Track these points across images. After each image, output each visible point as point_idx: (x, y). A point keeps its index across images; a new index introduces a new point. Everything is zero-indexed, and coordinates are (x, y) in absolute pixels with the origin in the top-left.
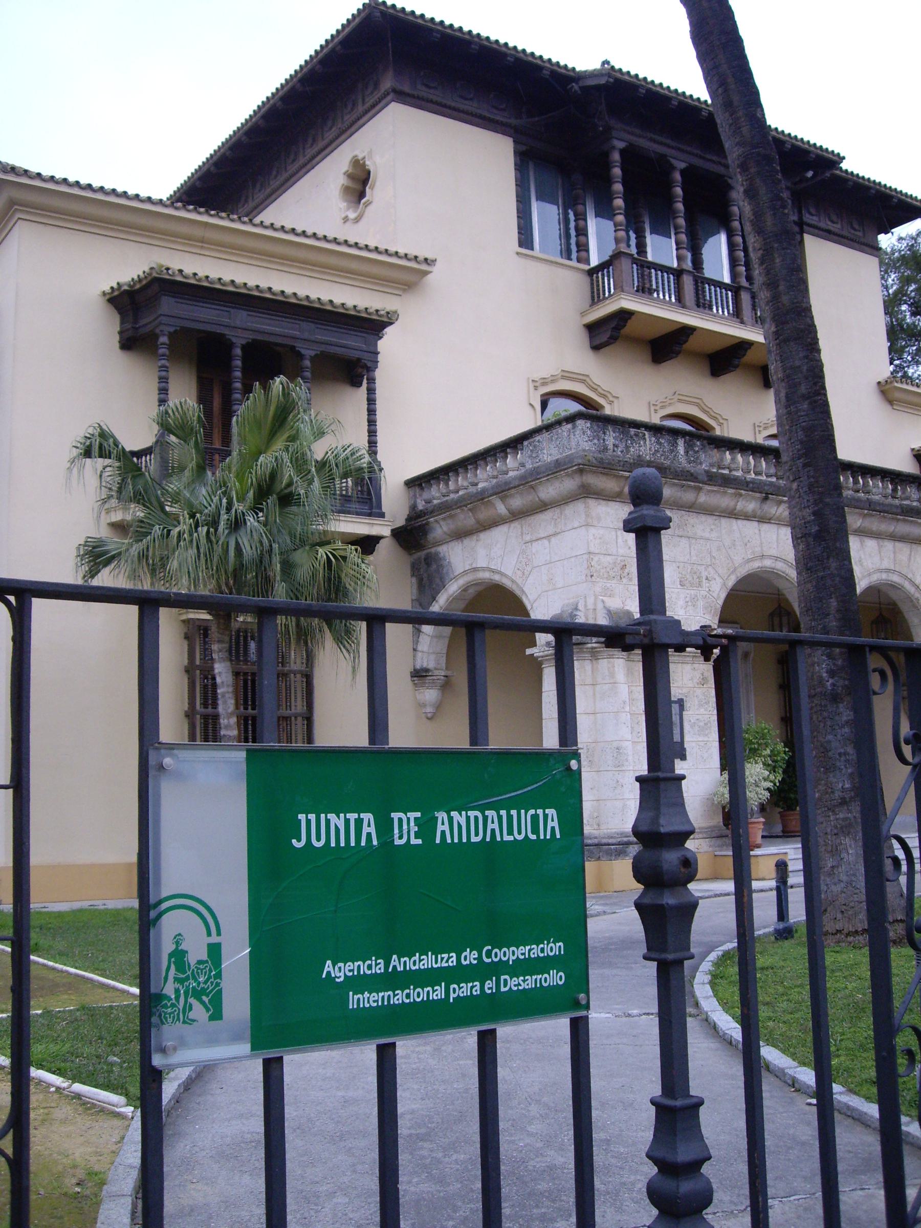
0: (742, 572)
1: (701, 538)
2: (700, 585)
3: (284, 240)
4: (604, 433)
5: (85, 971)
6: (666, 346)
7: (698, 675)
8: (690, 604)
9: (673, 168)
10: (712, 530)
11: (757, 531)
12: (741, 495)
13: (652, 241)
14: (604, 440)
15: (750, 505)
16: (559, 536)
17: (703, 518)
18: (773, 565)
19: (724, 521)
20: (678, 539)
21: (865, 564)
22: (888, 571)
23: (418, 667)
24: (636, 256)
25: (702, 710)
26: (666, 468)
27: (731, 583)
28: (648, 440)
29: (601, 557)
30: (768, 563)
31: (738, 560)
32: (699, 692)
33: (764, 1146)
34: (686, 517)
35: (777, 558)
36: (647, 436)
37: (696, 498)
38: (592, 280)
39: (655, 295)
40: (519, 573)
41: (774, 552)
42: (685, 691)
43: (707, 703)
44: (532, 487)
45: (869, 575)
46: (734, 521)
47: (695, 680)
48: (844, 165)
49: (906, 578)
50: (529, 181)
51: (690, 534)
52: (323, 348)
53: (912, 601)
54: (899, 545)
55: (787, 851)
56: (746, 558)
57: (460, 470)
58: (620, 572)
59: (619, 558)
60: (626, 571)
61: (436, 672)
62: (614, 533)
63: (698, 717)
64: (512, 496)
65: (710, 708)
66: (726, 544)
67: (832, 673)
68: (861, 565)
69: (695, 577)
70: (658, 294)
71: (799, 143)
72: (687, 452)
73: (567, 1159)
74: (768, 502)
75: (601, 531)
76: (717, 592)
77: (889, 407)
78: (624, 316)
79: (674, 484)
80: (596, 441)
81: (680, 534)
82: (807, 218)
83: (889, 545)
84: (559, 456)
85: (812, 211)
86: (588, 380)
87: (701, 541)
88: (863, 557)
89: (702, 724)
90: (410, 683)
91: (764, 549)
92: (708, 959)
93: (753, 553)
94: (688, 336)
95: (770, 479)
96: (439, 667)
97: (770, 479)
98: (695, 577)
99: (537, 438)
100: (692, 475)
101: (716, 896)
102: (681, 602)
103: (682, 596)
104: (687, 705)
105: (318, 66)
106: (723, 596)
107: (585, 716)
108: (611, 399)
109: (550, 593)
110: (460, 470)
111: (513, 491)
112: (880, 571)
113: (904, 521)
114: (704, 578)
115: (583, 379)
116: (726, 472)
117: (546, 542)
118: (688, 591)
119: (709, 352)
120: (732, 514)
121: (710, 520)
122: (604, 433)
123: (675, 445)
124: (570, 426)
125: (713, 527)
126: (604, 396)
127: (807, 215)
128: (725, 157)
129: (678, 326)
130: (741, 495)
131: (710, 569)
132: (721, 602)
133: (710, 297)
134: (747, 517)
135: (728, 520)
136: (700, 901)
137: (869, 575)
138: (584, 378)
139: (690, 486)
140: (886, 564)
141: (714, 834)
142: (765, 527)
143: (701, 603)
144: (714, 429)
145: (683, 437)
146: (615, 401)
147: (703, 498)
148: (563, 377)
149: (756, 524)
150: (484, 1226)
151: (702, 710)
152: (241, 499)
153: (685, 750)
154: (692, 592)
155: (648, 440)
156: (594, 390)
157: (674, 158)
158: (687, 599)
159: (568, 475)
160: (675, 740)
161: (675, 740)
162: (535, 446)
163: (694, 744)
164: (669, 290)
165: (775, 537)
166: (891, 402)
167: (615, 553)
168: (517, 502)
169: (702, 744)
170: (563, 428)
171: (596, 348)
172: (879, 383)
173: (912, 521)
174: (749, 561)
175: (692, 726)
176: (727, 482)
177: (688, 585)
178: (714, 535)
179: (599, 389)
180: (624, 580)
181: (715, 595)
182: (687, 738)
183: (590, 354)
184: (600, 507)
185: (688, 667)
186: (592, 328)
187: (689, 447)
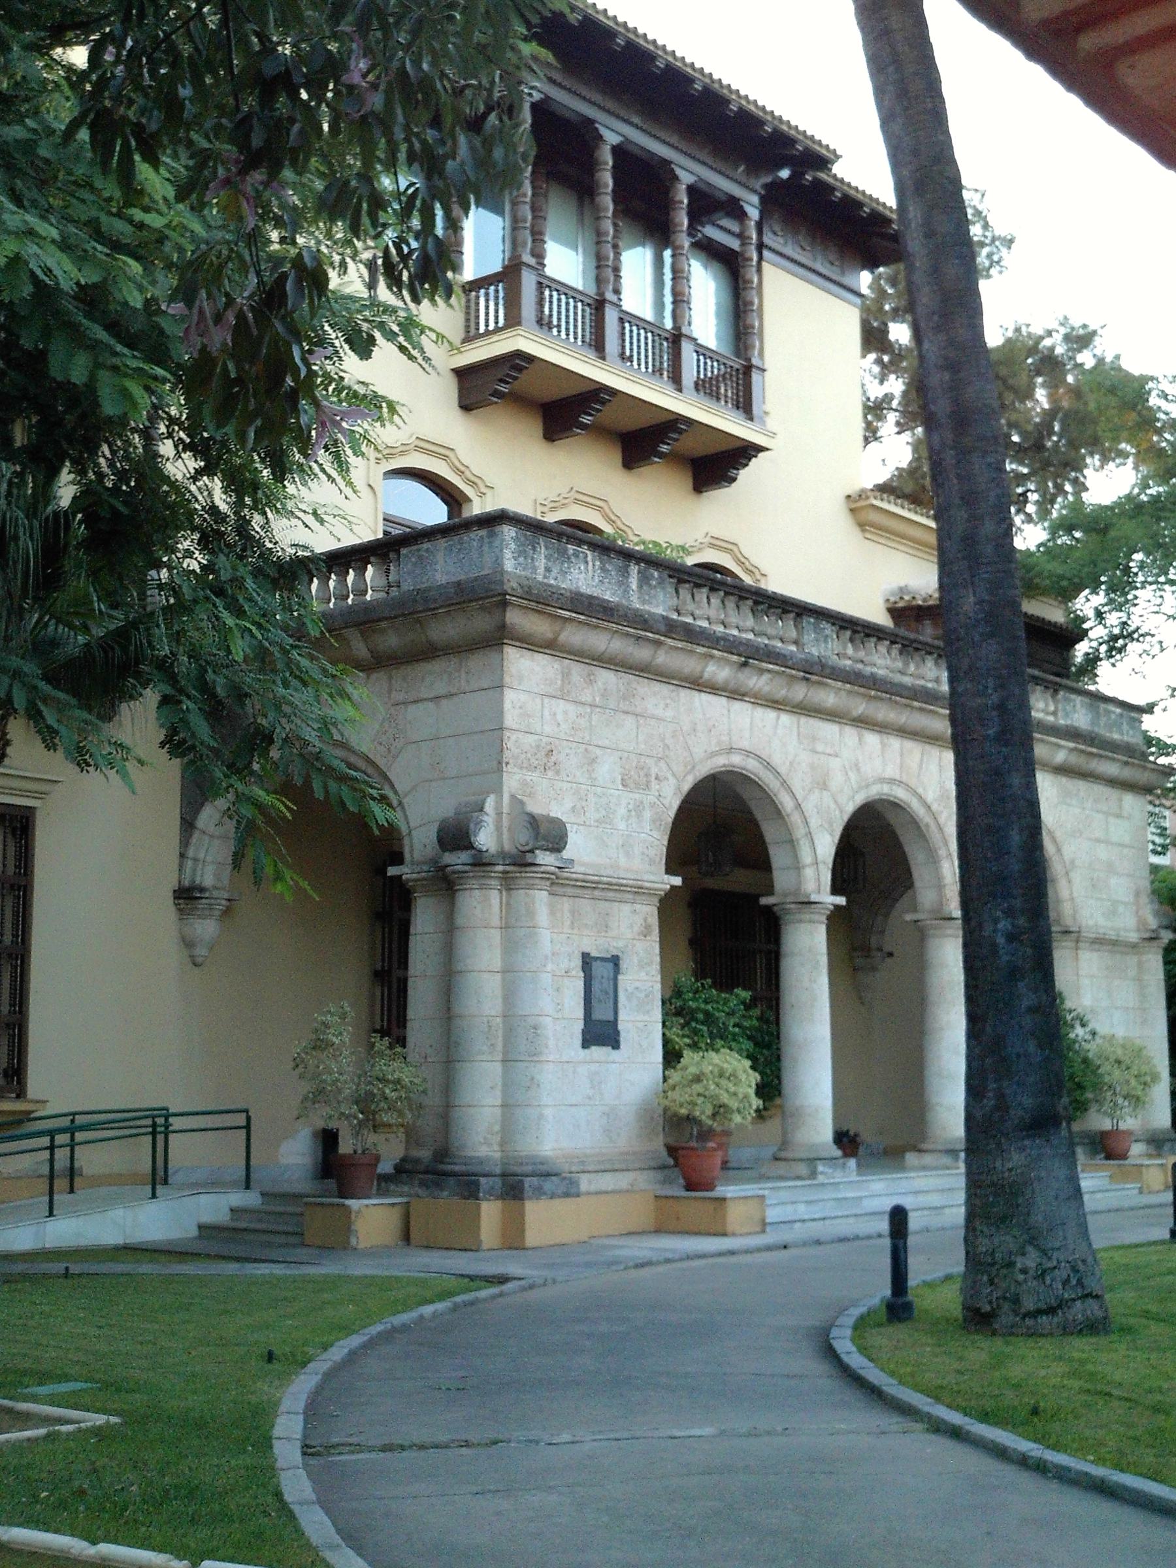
0: (704, 770)
1: (653, 717)
2: (648, 786)
3: (901, 517)
4: (534, 549)
5: (46, 1527)
6: (565, 412)
7: (639, 920)
8: (633, 813)
9: (676, 178)
10: (667, 705)
11: (725, 712)
12: (712, 657)
13: (477, 227)
14: (533, 559)
15: (719, 671)
16: (455, 699)
17: (657, 687)
18: (743, 764)
19: (684, 693)
20: (623, 716)
21: (862, 770)
22: (891, 781)
23: (187, 883)
24: (377, 335)
25: (643, 974)
26: (611, 609)
27: (687, 786)
28: (590, 564)
29: (520, 735)
30: (736, 760)
31: (699, 752)
32: (640, 946)
33: (662, 984)
34: (634, 685)
35: (748, 753)
36: (589, 558)
37: (653, 657)
38: (468, 301)
39: (555, 331)
40: (382, 749)
41: (745, 744)
42: (621, 944)
43: (650, 964)
44: (418, 621)
45: (867, 786)
46: (696, 693)
47: (636, 929)
48: (838, 169)
49: (915, 793)
50: (503, 204)
51: (638, 710)
52: (815, 1182)
53: (919, 827)
54: (909, 744)
55: (766, 1192)
56: (710, 751)
57: (392, 555)
58: (545, 760)
59: (545, 740)
60: (553, 759)
61: (215, 894)
62: (538, 701)
63: (637, 984)
64: (383, 631)
65: (654, 973)
66: (685, 728)
67: (1011, 937)
68: (858, 770)
69: (642, 773)
70: (559, 332)
71: (785, 128)
72: (640, 587)
73: (200, 1117)
74: (747, 670)
75: (523, 697)
76: (669, 798)
77: (856, 531)
78: (518, 361)
79: (628, 635)
80: (521, 559)
81: (625, 708)
82: (768, 239)
83: (895, 743)
84: (463, 577)
85: (777, 228)
86: (606, 508)
87: (653, 722)
88: (860, 758)
89: (642, 995)
90: (173, 908)
91: (734, 738)
92: (366, 1331)
93: (719, 743)
94: (750, 460)
95: (744, 635)
96: (219, 885)
97: (744, 635)
98: (642, 773)
99: (425, 546)
100: (646, 621)
101: (689, 1257)
102: (622, 811)
103: (624, 802)
104: (624, 965)
105: (838, 194)
106: (676, 804)
107: (954, 915)
108: (483, 490)
109: (434, 784)
110: (392, 555)
111: (384, 624)
112: (882, 780)
113: (921, 709)
114: (653, 776)
115: (442, 452)
116: (689, 620)
117: (431, 705)
118: (631, 795)
119: (546, 400)
120: (697, 684)
121: (664, 689)
122: (534, 549)
123: (625, 573)
124: (483, 533)
125: (668, 701)
126: (473, 484)
127: (770, 234)
128: (1025, 623)
129: (593, 387)
130: (712, 657)
131: (662, 764)
132: (672, 813)
133: (631, 350)
134: (713, 688)
135: (688, 691)
136: (1167, 1236)
137: (867, 786)
138: (730, 546)
139: (648, 639)
140: (891, 771)
141: (653, 1164)
142: (737, 706)
143: (647, 814)
144: (469, 500)
145: (637, 563)
146: (489, 492)
147: (662, 658)
148: (418, 448)
149: (724, 700)
150: (8, 1257)
151: (643, 974)
152: (726, 1002)
153: (617, 1033)
154: (637, 796)
155: (590, 564)
156: (740, 563)
157: (680, 167)
158: (630, 807)
159: (483, 608)
160: (844, 903)
161: (844, 903)
162: (420, 557)
163: (630, 1025)
164: (497, 298)
165: (748, 720)
166: (862, 526)
167: (539, 731)
168: (391, 640)
169: (640, 1025)
170: (472, 535)
171: (466, 406)
172: (849, 496)
173: (931, 711)
174: (713, 754)
175: (629, 998)
176: (692, 635)
177: (632, 786)
178: (669, 714)
179: (467, 473)
180: (550, 774)
181: (666, 802)
182: (622, 1016)
183: (456, 412)
184: (522, 660)
185: (626, 908)
186: (463, 374)
187: (644, 579)
